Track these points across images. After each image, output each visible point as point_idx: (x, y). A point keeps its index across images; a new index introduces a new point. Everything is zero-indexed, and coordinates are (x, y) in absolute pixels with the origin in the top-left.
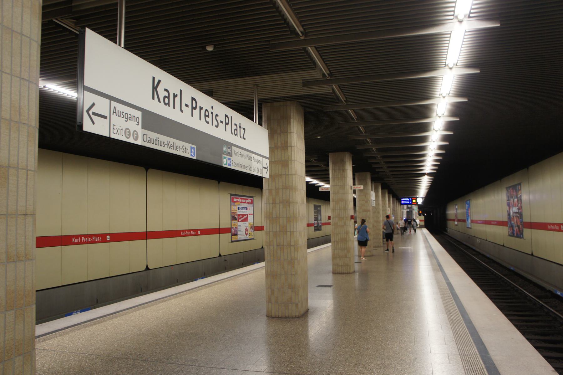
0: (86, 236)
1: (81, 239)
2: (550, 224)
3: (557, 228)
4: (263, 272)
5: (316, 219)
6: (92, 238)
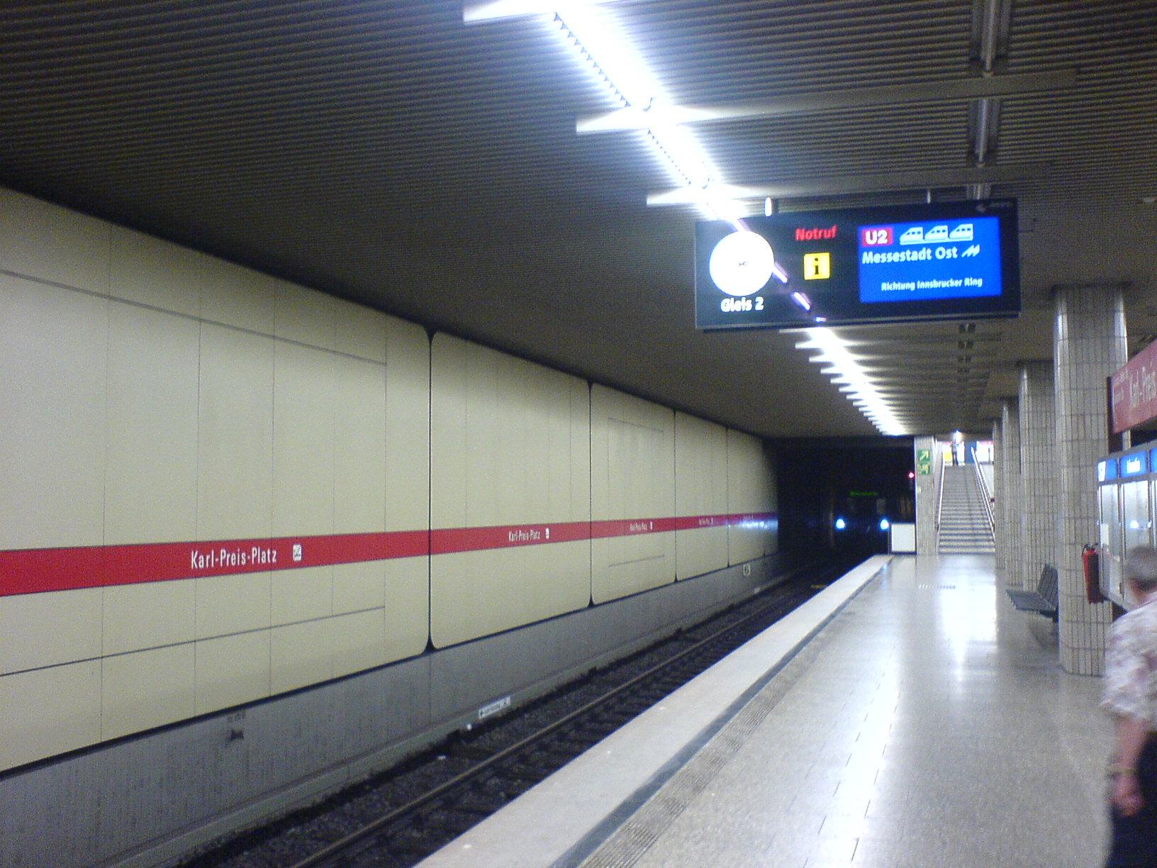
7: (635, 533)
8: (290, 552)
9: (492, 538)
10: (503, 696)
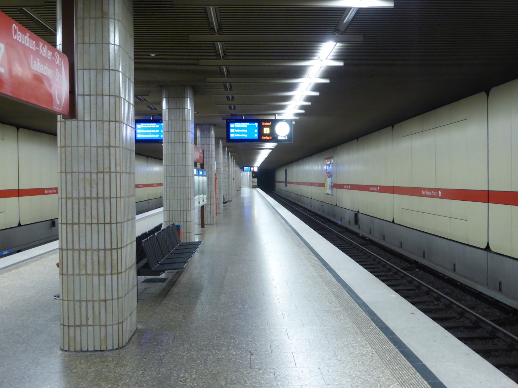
2: (425, 189)
3: (434, 194)
4: (56, 258)
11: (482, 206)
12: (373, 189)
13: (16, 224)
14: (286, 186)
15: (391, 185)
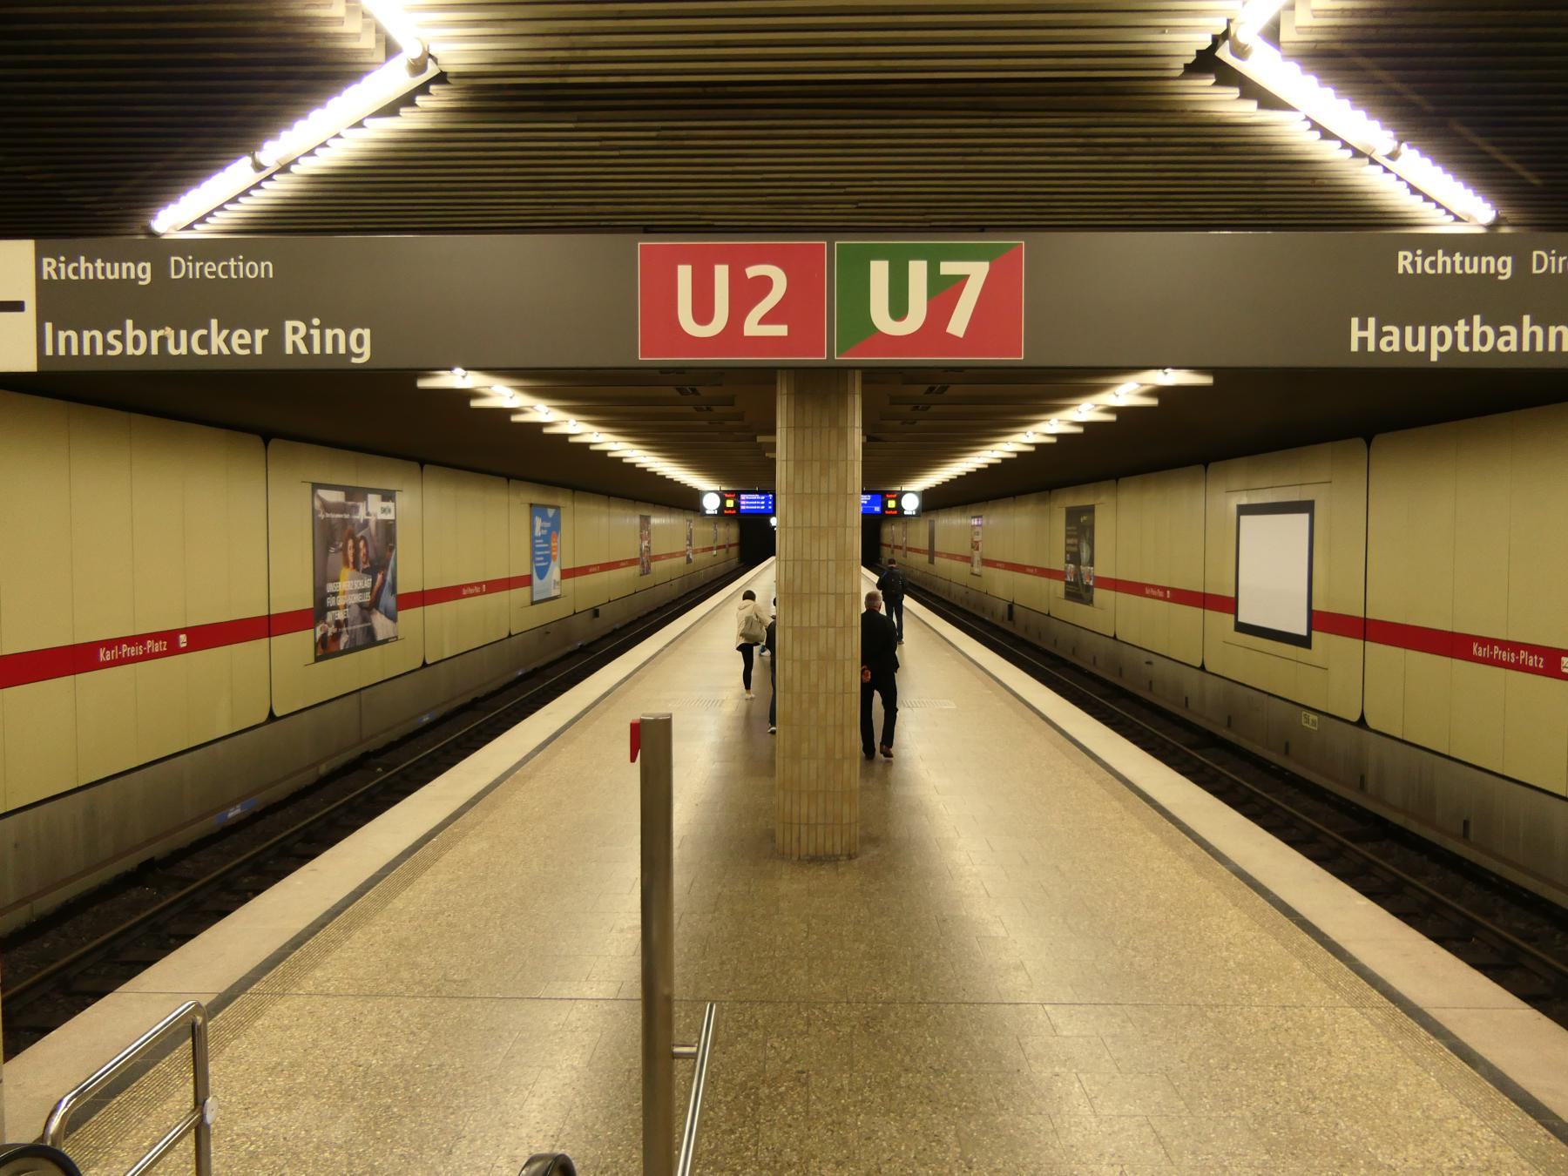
0: (1506, 645)
1: (1492, 649)
5: (1074, 558)
6: (1518, 654)
7: (469, 596)
8: (177, 641)
9: (452, 593)
10: (233, 804)
11: (1197, 612)
12: (1154, 592)
13: (264, 716)
14: (931, 561)
15: (1113, 576)
